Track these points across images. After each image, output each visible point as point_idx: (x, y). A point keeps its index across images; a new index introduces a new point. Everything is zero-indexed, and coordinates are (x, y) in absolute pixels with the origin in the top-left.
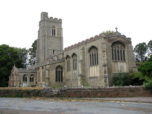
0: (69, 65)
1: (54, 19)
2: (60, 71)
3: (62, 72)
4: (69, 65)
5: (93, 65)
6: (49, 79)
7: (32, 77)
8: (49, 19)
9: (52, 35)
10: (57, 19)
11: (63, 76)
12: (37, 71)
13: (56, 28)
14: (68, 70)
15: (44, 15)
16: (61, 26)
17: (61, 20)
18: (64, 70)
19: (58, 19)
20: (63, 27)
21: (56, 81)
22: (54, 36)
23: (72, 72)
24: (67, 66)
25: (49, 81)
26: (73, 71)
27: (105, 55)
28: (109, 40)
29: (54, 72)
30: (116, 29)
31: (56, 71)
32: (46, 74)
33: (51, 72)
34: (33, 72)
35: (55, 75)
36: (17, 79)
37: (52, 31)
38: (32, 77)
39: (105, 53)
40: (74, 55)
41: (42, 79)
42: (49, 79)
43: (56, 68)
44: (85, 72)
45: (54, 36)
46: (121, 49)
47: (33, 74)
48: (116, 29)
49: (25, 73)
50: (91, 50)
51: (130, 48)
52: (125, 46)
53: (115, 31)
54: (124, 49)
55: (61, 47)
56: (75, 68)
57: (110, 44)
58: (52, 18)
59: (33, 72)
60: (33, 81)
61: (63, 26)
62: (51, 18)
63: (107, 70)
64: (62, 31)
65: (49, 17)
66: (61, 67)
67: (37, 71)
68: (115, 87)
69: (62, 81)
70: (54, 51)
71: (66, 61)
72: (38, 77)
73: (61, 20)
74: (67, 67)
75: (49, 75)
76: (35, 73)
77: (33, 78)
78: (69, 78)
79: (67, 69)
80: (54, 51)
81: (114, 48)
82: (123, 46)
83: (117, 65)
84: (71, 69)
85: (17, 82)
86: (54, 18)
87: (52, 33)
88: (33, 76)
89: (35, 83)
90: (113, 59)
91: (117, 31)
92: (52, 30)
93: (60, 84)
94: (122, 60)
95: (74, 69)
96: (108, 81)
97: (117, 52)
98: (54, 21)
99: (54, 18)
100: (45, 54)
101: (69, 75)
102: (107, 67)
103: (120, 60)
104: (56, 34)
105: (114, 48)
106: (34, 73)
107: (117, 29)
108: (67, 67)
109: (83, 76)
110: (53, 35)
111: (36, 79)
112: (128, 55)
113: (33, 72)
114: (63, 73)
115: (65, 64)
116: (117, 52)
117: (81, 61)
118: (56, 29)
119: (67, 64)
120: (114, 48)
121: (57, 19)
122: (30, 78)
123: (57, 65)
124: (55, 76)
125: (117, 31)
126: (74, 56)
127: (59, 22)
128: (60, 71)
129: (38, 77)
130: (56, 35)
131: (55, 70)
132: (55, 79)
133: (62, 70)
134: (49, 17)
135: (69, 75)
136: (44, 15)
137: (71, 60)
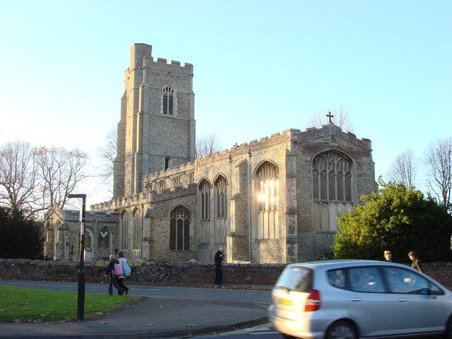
0: (207, 206)
1: (168, 66)
2: (184, 220)
3: (187, 223)
4: (207, 206)
5: (330, 198)
6: (151, 241)
7: (104, 236)
8: (155, 63)
9: (162, 112)
10: (178, 64)
11: (192, 233)
12: (120, 219)
13: (175, 91)
14: (203, 218)
15: (143, 51)
16: (190, 84)
17: (189, 67)
18: (193, 218)
19: (182, 65)
20: (195, 89)
21: (172, 247)
22: (168, 115)
23: (215, 226)
24: (201, 207)
25: (151, 248)
26: (218, 223)
27: (294, 188)
28: (305, 148)
29: (165, 224)
30: (330, 116)
31: (173, 222)
32: (144, 229)
33: (157, 222)
34: (108, 222)
35: (169, 231)
36: (64, 241)
37: (162, 102)
38: (104, 236)
39: (295, 182)
40: (220, 179)
41: (132, 241)
42: (151, 241)
43: (172, 213)
44: (246, 227)
45: (168, 115)
46: (341, 169)
47: (109, 225)
48: (330, 116)
49: (105, 224)
50: (263, 171)
51: (365, 168)
52: (350, 161)
53: (326, 122)
54: (350, 169)
55: (189, 148)
56: (207, 216)
57: (308, 159)
58: (165, 61)
59: (108, 222)
60: (107, 245)
61: (197, 85)
62: (162, 61)
63: (296, 226)
64: (193, 101)
65: (155, 60)
66: (186, 209)
67: (120, 219)
68: (39, 187)
69: (187, 247)
70: (167, 160)
71: (199, 193)
72: (121, 235)
73: (189, 67)
74: (203, 210)
75: (152, 231)
76: (114, 225)
77: (108, 237)
78: (207, 241)
79: (201, 216)
80: (167, 160)
81: (319, 168)
82: (346, 163)
83: (328, 210)
84: (213, 215)
85: (63, 248)
86: (169, 62)
87: (162, 107)
88: (107, 233)
89: (113, 251)
90: (316, 196)
91: (330, 121)
92: (162, 98)
93: (181, 255)
94: (340, 198)
95: (219, 216)
96: (296, 251)
97: (328, 177)
98: (169, 69)
99: (169, 62)
100: (141, 168)
101: (206, 231)
102: (296, 216)
103: (336, 199)
104: (175, 109)
105: (322, 168)
106: (111, 225)
107: (333, 116)
108: (203, 210)
109: (239, 236)
110: (165, 112)
111: (114, 242)
112: (358, 186)
113: (107, 219)
114: (191, 226)
115: (195, 203)
116: (328, 177)
117: (237, 198)
118: (175, 95)
119: (201, 203)
120: (319, 168)
121: (179, 63)
122: (100, 238)
123: (175, 203)
124: (168, 234)
125: (330, 121)
126: (221, 183)
127: (186, 72)
128: (184, 220)
129: (121, 235)
130: (175, 113)
131: (169, 219)
132: (168, 241)
133: (189, 217)
134: (155, 60)
135: (206, 231)
136: (143, 51)
137: (212, 190)
